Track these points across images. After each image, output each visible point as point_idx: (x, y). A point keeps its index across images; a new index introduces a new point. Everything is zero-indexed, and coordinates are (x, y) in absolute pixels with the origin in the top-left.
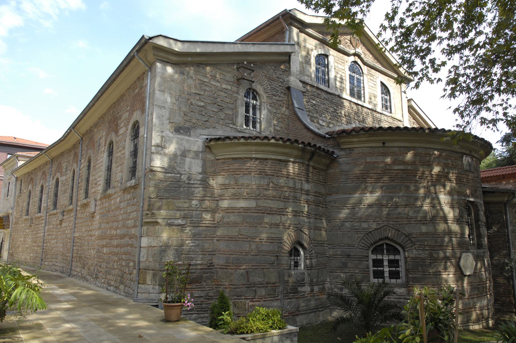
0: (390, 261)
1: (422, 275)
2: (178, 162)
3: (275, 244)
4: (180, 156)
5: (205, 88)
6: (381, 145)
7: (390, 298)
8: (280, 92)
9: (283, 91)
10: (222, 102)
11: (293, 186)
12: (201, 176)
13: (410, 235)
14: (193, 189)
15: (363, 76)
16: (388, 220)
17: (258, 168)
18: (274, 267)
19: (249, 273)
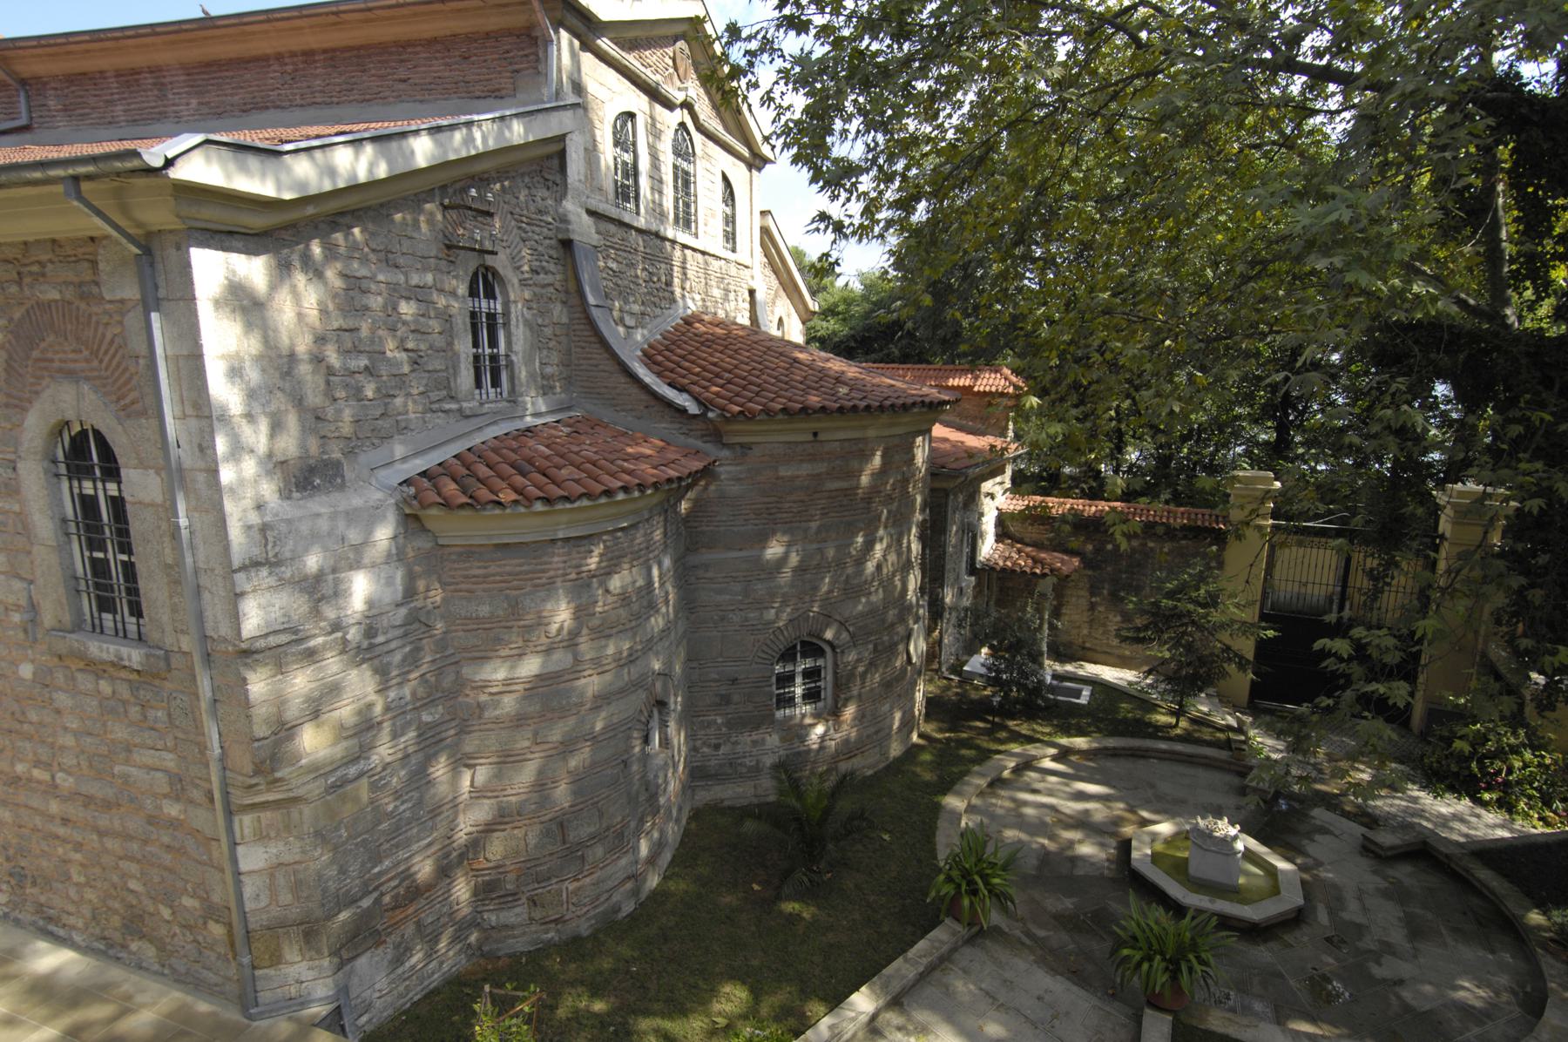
6: (810, 438)
9: (553, 253)
15: (694, 162)
19: (565, 824)
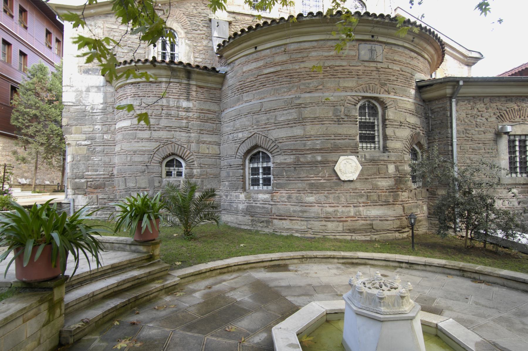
0: (264, 168)
1: (287, 180)
2: (84, 96)
3: (146, 155)
4: (85, 91)
5: (114, 34)
6: (253, 50)
7: (257, 203)
8: (202, 26)
10: (133, 43)
11: (167, 104)
12: (102, 106)
13: (276, 140)
14: (96, 117)
16: (258, 127)
17: (133, 91)
18: (144, 175)
